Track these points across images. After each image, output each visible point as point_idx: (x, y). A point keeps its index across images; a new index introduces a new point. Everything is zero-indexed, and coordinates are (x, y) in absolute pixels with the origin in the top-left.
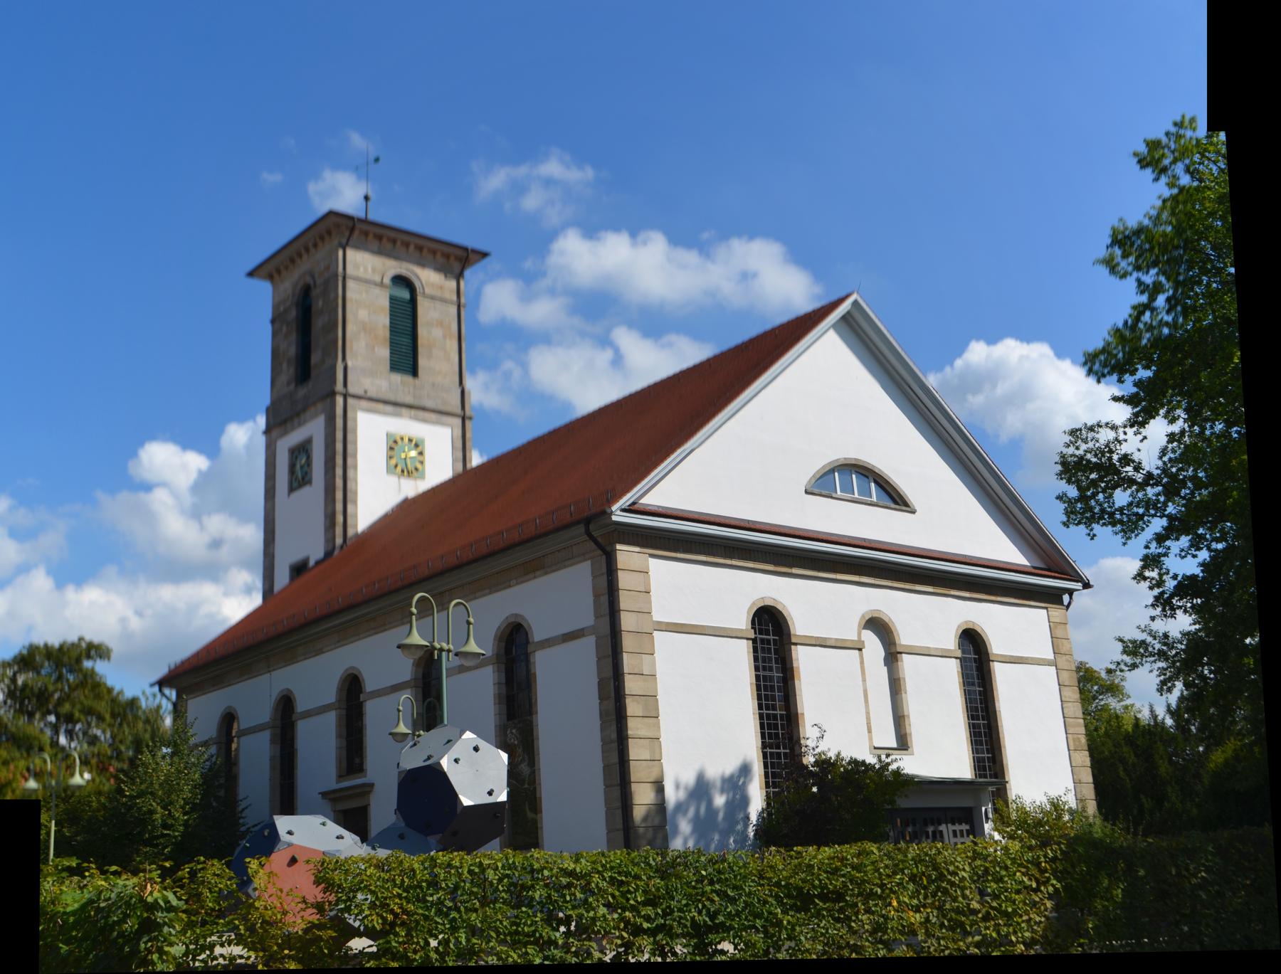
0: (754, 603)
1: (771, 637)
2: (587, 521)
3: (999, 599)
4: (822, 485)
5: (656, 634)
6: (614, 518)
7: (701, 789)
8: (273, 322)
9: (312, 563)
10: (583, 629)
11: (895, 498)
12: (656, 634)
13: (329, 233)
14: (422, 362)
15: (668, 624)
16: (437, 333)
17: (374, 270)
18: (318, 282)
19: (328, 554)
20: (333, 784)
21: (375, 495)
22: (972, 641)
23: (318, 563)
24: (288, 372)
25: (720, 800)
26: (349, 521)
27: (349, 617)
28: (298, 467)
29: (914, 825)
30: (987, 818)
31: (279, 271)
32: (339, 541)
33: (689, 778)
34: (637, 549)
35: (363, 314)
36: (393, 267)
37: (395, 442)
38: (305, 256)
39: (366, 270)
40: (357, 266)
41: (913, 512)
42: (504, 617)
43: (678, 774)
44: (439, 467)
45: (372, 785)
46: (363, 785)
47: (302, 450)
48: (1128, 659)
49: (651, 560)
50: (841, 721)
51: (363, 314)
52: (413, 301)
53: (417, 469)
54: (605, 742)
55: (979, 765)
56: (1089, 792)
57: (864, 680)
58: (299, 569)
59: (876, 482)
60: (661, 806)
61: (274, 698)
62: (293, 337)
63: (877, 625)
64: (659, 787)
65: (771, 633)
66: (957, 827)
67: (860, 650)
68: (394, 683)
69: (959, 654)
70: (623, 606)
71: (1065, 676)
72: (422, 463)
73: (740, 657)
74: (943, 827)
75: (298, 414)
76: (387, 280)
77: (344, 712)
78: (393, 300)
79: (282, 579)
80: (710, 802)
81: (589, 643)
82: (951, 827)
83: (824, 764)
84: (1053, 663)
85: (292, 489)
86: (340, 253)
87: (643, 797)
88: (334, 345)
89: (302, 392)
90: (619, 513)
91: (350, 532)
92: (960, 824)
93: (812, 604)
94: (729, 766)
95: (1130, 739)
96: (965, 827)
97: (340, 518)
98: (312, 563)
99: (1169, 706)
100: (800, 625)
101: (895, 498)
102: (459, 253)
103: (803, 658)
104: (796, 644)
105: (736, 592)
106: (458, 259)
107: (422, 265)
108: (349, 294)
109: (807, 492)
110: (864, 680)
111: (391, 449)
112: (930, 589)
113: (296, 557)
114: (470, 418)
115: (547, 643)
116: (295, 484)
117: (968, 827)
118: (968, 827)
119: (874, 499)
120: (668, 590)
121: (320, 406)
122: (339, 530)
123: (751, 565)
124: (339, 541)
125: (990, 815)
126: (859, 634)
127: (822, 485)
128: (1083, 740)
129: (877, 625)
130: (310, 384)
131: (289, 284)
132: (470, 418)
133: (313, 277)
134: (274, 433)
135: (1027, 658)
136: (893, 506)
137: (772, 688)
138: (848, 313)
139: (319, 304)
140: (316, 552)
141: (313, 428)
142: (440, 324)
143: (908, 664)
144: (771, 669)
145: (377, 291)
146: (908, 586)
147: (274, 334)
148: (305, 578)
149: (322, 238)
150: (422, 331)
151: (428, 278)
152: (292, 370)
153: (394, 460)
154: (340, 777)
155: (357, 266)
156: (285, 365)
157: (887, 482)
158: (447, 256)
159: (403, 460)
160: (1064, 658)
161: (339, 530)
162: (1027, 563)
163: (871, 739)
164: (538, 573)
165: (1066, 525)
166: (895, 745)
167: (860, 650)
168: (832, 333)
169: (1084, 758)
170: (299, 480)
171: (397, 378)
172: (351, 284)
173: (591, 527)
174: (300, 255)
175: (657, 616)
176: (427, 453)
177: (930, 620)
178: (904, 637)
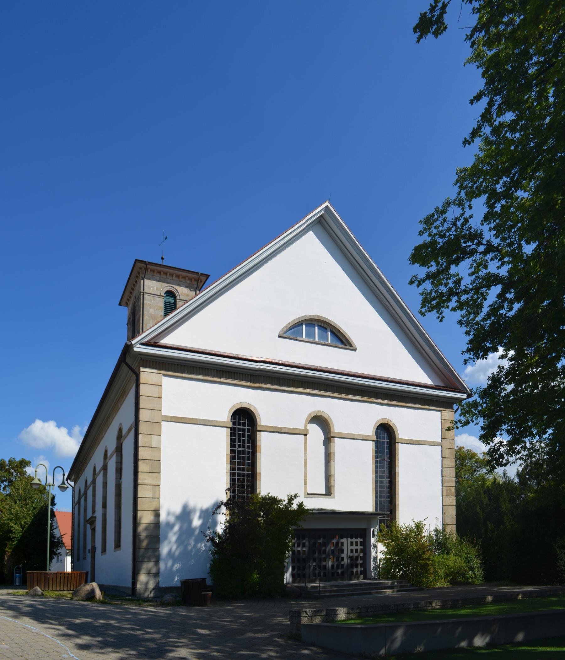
0: (234, 406)
1: (246, 428)
3: (408, 405)
4: (293, 331)
5: (163, 423)
6: (135, 349)
7: (185, 514)
11: (342, 340)
12: (163, 423)
15: (172, 417)
17: (157, 289)
22: (386, 431)
25: (197, 522)
29: (324, 538)
30: (374, 535)
33: (177, 509)
34: (155, 371)
35: (152, 311)
39: (153, 289)
40: (149, 288)
41: (355, 350)
43: (170, 506)
48: (463, 419)
49: (164, 378)
50: (284, 476)
51: (152, 311)
55: (378, 503)
56: (452, 520)
57: (306, 454)
59: (332, 332)
60: (157, 525)
63: (320, 420)
64: (157, 514)
65: (244, 424)
66: (354, 540)
67: (305, 435)
69: (375, 438)
70: (141, 407)
71: (447, 452)
73: (221, 440)
74: (344, 540)
76: (163, 294)
78: (166, 303)
80: (190, 522)
82: (350, 540)
83: (271, 502)
84: (441, 444)
86: (142, 281)
87: (146, 518)
90: (139, 346)
92: (356, 538)
93: (268, 405)
94: (207, 503)
95: (488, 491)
96: (359, 540)
99: (518, 471)
100: (264, 419)
101: (342, 340)
102: (196, 276)
103: (264, 440)
104: (260, 431)
105: (226, 398)
107: (180, 286)
108: (145, 302)
109: (280, 337)
110: (306, 454)
112: (360, 398)
115: (364, 439)
117: (361, 540)
118: (361, 540)
119: (329, 341)
120: (172, 394)
123: (234, 382)
125: (376, 533)
126: (306, 426)
127: (293, 331)
128: (453, 490)
129: (320, 420)
135: (422, 441)
136: (340, 346)
137: (244, 458)
138: (321, 216)
143: (337, 444)
144: (244, 446)
146: (344, 396)
155: (149, 288)
157: (339, 331)
158: (191, 279)
160: (448, 441)
162: (427, 381)
163: (306, 489)
165: (423, 314)
166: (324, 493)
167: (305, 435)
168: (311, 234)
169: (452, 501)
172: (146, 297)
175: (164, 412)
177: (357, 418)
178: (337, 428)
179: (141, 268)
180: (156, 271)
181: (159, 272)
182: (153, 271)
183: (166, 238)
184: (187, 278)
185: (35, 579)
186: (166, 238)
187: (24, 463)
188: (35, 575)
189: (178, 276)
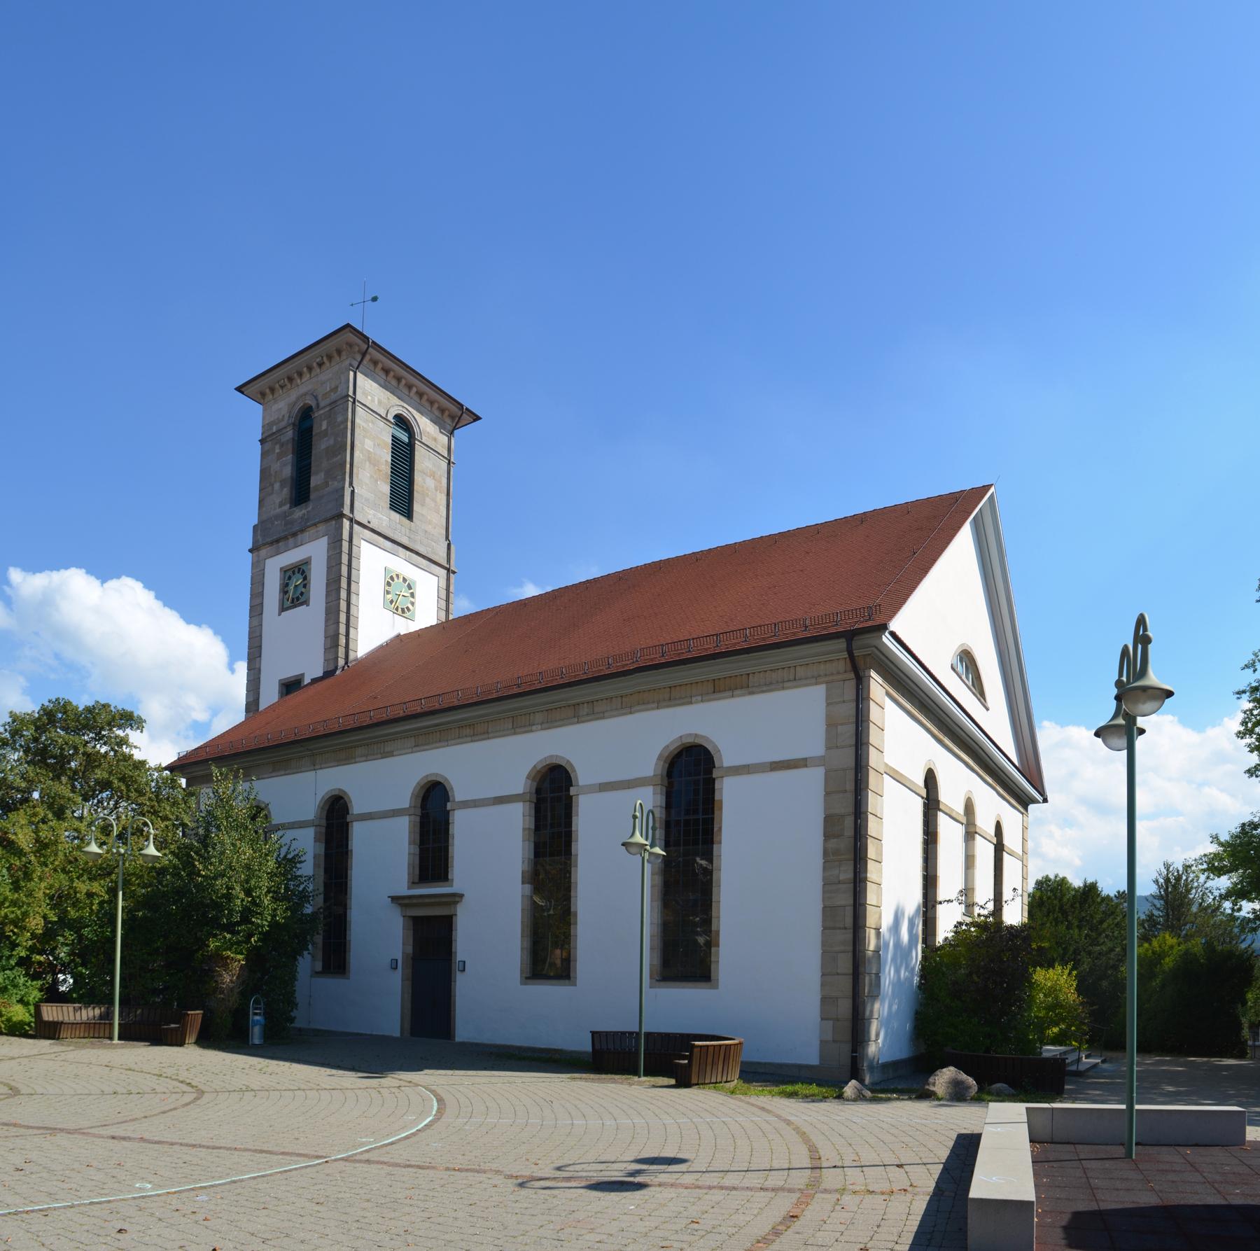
2: (850, 636)
8: (262, 441)
9: (307, 681)
10: (805, 759)
13: (339, 352)
14: (416, 507)
16: (430, 483)
18: (322, 404)
19: (328, 674)
20: (403, 889)
21: (373, 628)
23: (314, 681)
24: (282, 493)
26: (351, 646)
27: (407, 727)
28: (292, 588)
31: (272, 390)
32: (341, 662)
36: (395, 406)
37: (392, 578)
38: (306, 376)
39: (373, 401)
40: (365, 394)
42: (676, 736)
44: (426, 615)
45: (461, 896)
46: (454, 895)
47: (300, 569)
52: (411, 446)
53: (408, 609)
54: (829, 885)
58: (290, 686)
61: (319, 798)
62: (289, 458)
68: (613, 779)
72: (413, 604)
75: (294, 535)
76: (390, 417)
77: (418, 819)
79: (270, 695)
81: (814, 779)
85: (283, 609)
86: (886, 639)
88: (341, 468)
89: (299, 513)
91: (352, 656)
97: (342, 640)
98: (307, 681)
106: (452, 417)
107: (422, 413)
108: (357, 421)
111: (389, 584)
113: (290, 673)
114: (454, 572)
115: (466, 804)
116: (288, 604)
121: (322, 528)
122: (341, 651)
124: (341, 662)
130: (310, 506)
131: (284, 405)
132: (454, 572)
133: (316, 397)
134: (263, 552)
139: (321, 425)
140: (313, 669)
141: (314, 550)
142: (433, 475)
145: (381, 424)
147: (264, 455)
148: (296, 698)
149: (330, 358)
150: (418, 478)
151: (425, 426)
152: (286, 491)
153: (393, 597)
154: (413, 884)
156: (277, 486)
158: (442, 411)
159: (398, 597)
161: (341, 651)
164: (737, 692)
170: (294, 597)
171: (396, 517)
173: (855, 644)
174: (300, 375)
176: (416, 595)
179: (350, 345)
180: (380, 366)
181: (387, 371)
182: (375, 363)
183: (375, 299)
184: (436, 405)
185: (710, 1060)
186: (375, 299)
187: (130, 719)
188: (711, 1050)
189: (420, 394)
